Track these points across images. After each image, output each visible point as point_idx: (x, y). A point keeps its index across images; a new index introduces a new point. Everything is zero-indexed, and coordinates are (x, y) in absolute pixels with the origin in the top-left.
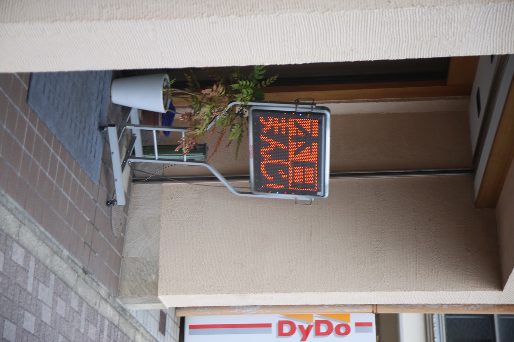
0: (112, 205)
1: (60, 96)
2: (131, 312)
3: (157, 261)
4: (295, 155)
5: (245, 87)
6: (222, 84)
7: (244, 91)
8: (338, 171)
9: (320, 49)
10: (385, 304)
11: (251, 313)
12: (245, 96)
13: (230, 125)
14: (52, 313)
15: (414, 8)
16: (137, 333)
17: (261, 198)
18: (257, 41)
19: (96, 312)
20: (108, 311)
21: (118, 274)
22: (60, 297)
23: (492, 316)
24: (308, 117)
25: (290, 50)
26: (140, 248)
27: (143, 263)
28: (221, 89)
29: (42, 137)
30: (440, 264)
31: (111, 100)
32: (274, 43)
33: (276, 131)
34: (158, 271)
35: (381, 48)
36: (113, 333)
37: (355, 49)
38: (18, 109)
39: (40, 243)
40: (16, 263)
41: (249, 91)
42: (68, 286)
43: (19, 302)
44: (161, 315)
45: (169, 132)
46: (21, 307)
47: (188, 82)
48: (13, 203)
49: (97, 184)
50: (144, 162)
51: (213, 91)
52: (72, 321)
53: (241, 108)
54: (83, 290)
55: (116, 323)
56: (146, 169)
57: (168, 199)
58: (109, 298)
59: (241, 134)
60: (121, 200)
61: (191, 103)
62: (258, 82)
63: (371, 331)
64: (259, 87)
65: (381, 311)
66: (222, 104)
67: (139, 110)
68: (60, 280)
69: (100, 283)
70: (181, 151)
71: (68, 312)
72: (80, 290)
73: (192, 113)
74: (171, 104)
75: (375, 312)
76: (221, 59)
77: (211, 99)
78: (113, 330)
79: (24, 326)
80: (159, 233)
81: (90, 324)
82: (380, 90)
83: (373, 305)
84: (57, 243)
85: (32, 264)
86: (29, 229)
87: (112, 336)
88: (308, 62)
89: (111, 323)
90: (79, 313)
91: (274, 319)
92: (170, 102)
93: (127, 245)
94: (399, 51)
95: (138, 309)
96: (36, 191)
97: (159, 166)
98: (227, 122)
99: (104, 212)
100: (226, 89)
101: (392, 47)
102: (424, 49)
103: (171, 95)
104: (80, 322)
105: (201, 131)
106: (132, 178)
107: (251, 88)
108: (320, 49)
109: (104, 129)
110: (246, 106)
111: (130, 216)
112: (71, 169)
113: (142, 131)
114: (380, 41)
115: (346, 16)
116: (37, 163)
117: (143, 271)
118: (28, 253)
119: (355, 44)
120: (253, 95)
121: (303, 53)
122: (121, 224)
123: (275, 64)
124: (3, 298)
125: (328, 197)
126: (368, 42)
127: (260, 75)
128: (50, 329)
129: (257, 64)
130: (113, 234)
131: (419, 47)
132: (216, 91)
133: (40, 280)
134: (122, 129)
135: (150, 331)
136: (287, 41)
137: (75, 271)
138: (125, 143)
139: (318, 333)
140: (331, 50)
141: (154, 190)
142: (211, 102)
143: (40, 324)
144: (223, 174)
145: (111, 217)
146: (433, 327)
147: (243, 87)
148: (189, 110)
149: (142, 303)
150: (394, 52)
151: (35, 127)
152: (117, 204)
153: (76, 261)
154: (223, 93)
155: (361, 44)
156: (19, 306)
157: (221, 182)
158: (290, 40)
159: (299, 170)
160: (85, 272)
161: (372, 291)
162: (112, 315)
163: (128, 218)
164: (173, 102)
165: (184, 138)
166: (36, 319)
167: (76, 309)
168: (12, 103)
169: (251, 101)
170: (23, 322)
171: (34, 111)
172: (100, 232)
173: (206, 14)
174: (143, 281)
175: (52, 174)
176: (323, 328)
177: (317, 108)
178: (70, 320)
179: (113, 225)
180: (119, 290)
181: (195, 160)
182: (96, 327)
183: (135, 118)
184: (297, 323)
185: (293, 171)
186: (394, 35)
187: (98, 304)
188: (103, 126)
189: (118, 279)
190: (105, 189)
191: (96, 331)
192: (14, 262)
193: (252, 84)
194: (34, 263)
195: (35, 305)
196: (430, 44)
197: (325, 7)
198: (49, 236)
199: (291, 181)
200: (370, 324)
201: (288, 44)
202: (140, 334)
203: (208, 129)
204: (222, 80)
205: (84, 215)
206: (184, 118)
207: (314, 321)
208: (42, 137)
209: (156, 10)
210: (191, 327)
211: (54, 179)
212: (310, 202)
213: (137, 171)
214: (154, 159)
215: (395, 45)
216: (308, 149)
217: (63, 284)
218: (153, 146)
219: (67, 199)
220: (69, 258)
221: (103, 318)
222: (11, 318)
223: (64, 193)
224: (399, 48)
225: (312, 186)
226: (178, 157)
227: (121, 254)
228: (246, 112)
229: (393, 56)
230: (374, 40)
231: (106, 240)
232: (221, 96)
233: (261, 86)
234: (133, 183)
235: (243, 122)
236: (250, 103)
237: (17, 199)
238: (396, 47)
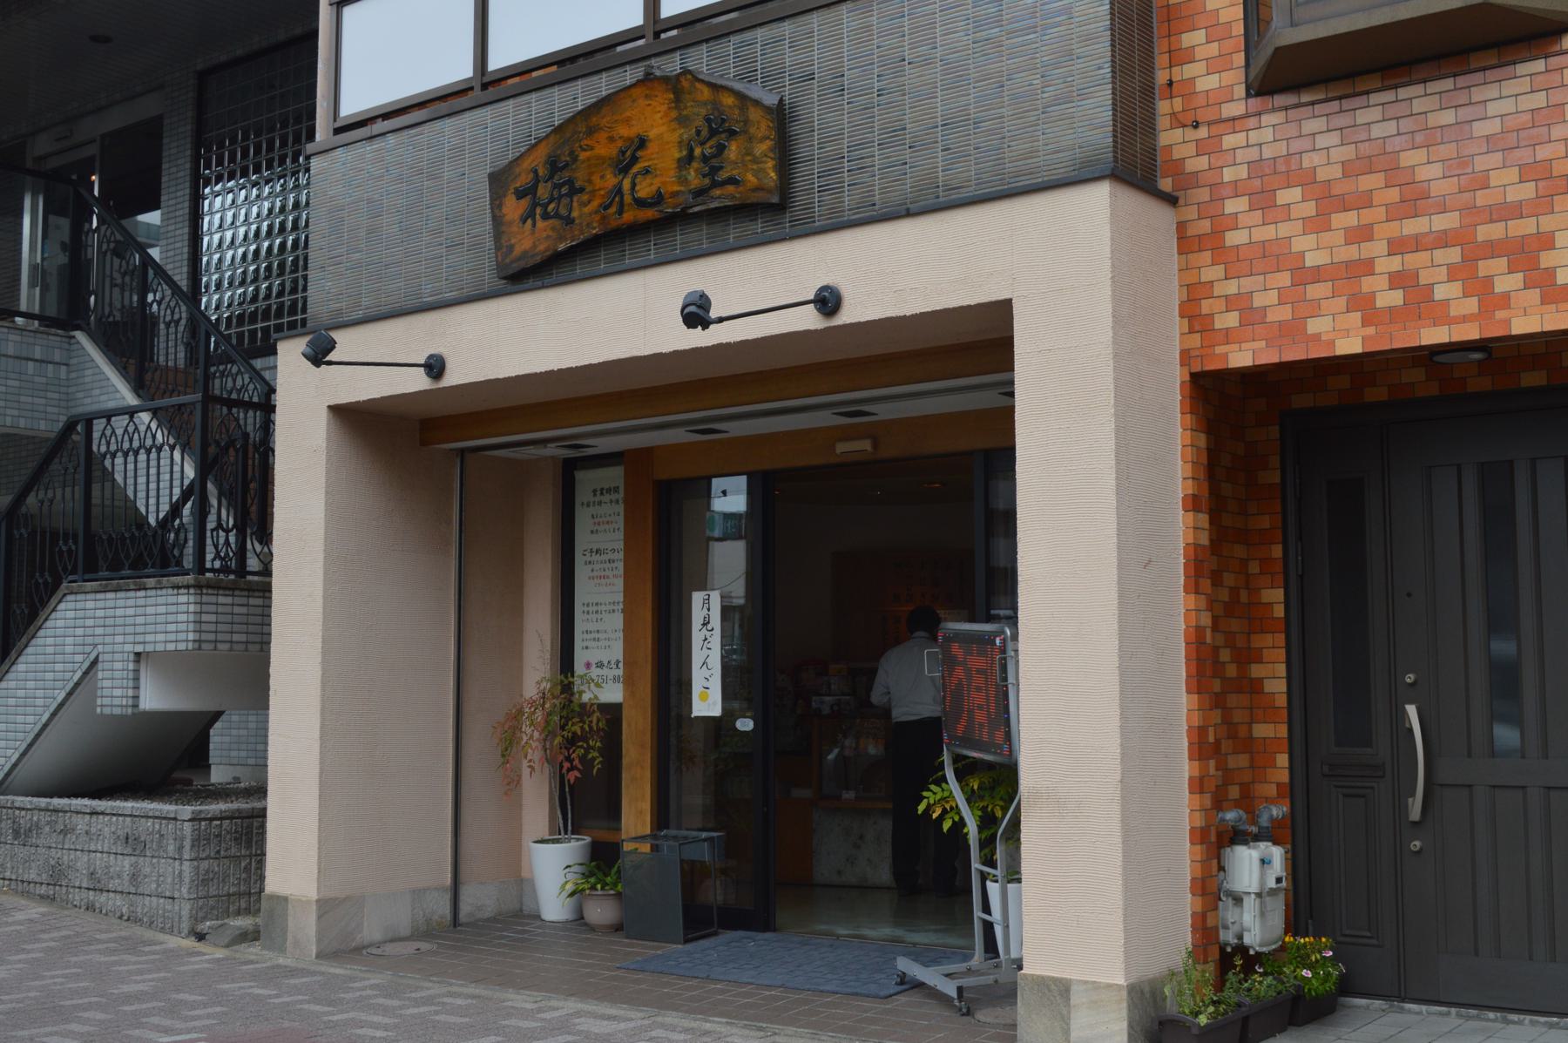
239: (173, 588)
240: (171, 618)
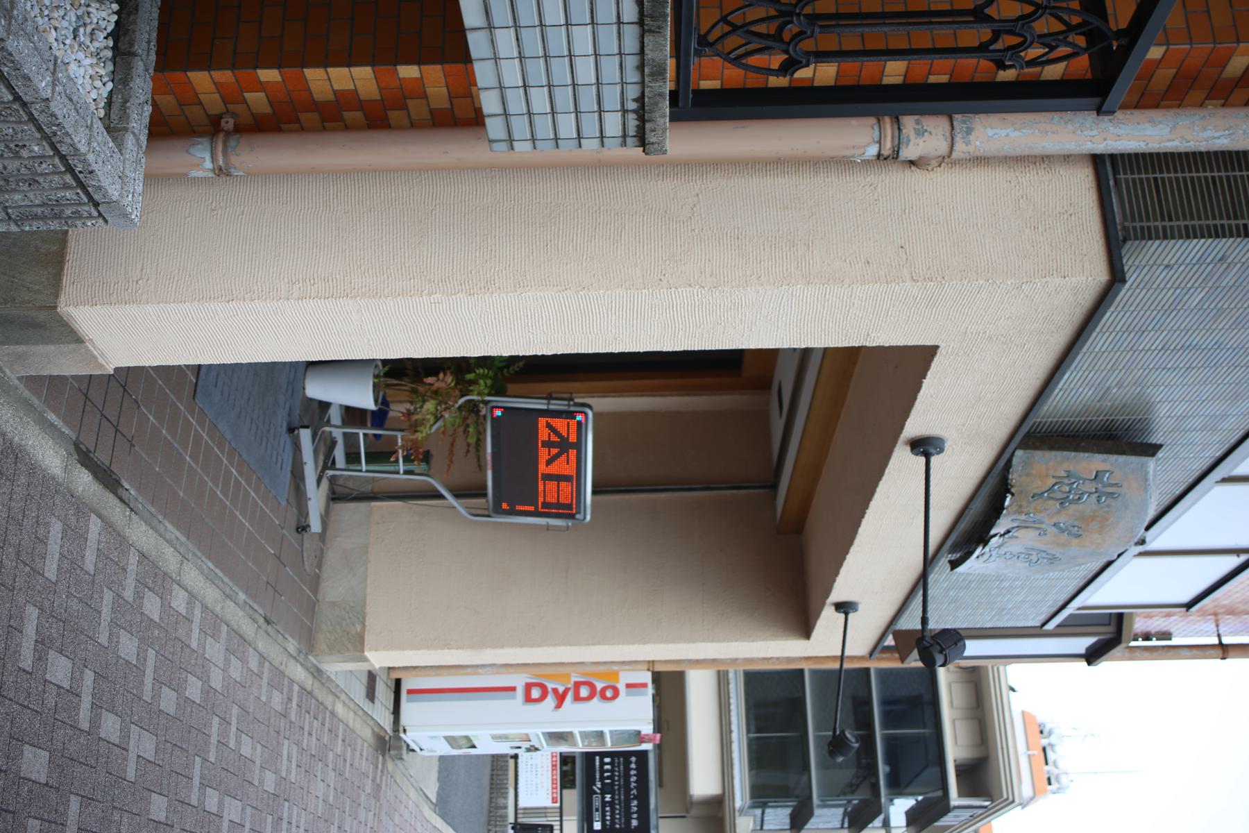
0: (303, 532)
1: (237, 390)
2: (328, 674)
3: (364, 606)
4: (547, 466)
6: (451, 373)
7: (481, 382)
12: (482, 388)
15: (692, 289)
16: (337, 700)
17: (501, 523)
19: (282, 674)
20: (298, 672)
21: (312, 623)
23: (802, 671)
27: (345, 609)
28: (449, 378)
29: (212, 444)
31: (304, 393)
34: (364, 618)
36: (304, 701)
38: (182, 408)
40: (177, 611)
42: (245, 641)
43: (181, 662)
44: (369, 677)
48: (172, 532)
52: (250, 687)
55: (309, 688)
56: (350, 484)
57: (378, 523)
58: (299, 655)
60: (315, 525)
63: (646, 694)
65: (658, 668)
67: (341, 406)
68: (235, 633)
69: (287, 636)
72: (261, 646)
74: (384, 398)
75: (651, 669)
78: (304, 697)
80: (367, 569)
82: (657, 382)
83: (649, 662)
84: (231, 584)
85: (197, 612)
87: (304, 705)
89: (302, 688)
90: (260, 676)
91: (519, 681)
93: (325, 585)
95: (338, 669)
97: (367, 480)
100: (457, 379)
104: (261, 688)
105: (424, 435)
106: (330, 495)
107: (490, 378)
112: (250, 485)
113: (345, 434)
115: (606, 297)
116: (206, 478)
117: (344, 619)
118: (192, 597)
120: (492, 387)
123: (517, 354)
124: (160, 657)
130: (305, 570)
132: (443, 381)
137: (255, 621)
138: (322, 449)
139: (577, 698)
143: (208, 691)
144: (451, 490)
146: (728, 684)
151: (204, 431)
153: (256, 607)
154: (453, 384)
156: (181, 668)
159: (552, 485)
160: (268, 622)
163: (324, 548)
168: (175, 400)
169: (490, 394)
171: (202, 410)
172: (287, 568)
173: (426, 292)
176: (584, 692)
177: (576, 405)
179: (305, 559)
182: (282, 693)
183: (335, 416)
184: (550, 686)
185: (544, 487)
187: (284, 663)
189: (312, 630)
190: (295, 510)
191: (282, 699)
197: (580, 285)
198: (220, 574)
200: (645, 685)
205: (266, 546)
207: (572, 683)
208: (212, 444)
209: (362, 287)
210: (410, 692)
211: (227, 500)
214: (361, 471)
216: (564, 457)
218: (359, 454)
219: (245, 525)
220: (246, 602)
221: (292, 681)
223: (241, 517)
225: (569, 507)
231: (296, 578)
237: (178, 527)
239: (641, 99)
240: (564, 98)
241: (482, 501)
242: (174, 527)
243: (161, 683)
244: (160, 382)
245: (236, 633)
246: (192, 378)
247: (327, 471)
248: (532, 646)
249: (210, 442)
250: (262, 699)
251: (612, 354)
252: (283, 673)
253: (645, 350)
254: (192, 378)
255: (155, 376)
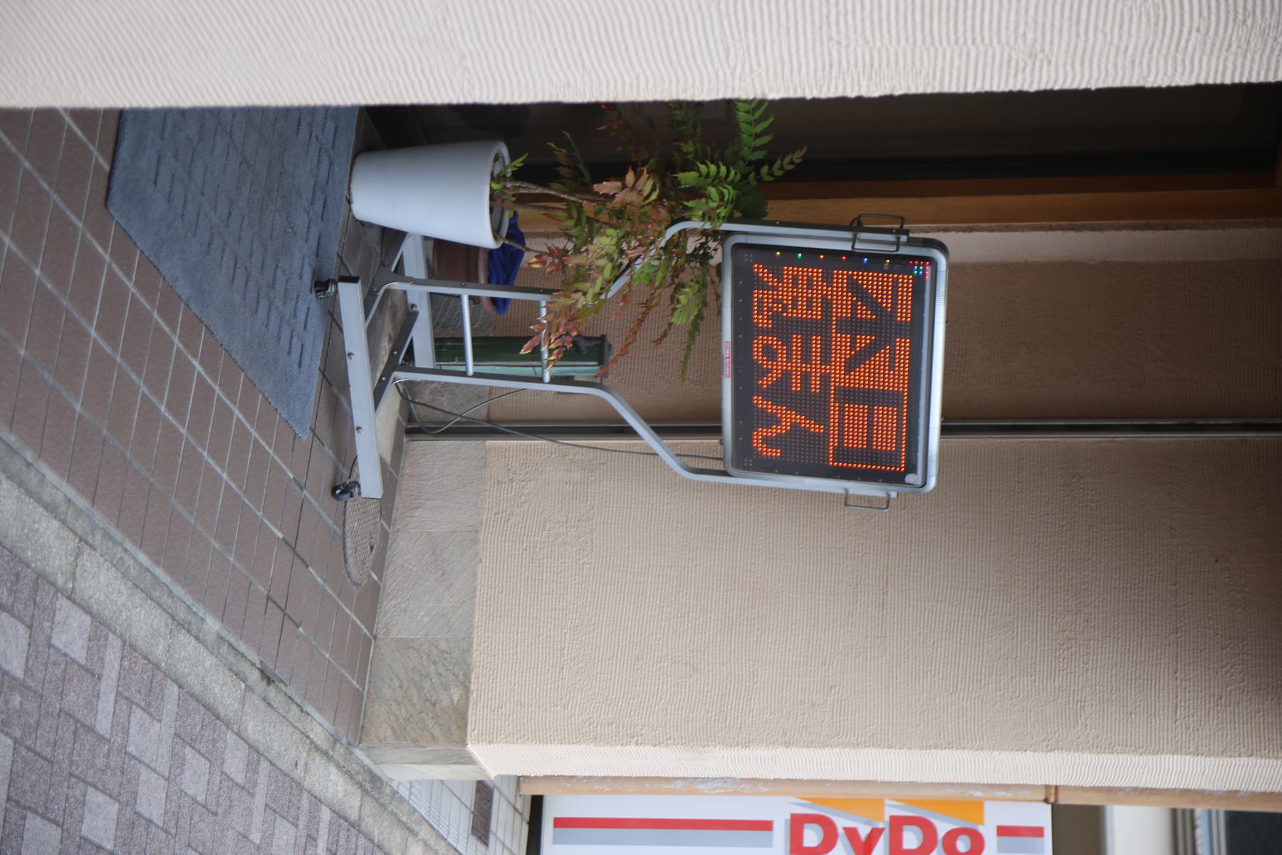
0: (346, 496)
2: (395, 784)
3: (468, 651)
4: (847, 372)
5: (714, 180)
7: (712, 191)
8: (965, 419)
9: (936, 51)
10: (1087, 784)
11: (717, 791)
12: (713, 205)
13: (670, 286)
14: (167, 794)
17: (750, 488)
18: (746, 24)
22: (193, 747)
24: (886, 267)
25: (843, 52)
26: (422, 613)
27: (428, 656)
28: (647, 184)
30: (1243, 680)
31: (350, 210)
32: (796, 30)
33: (796, 386)
34: (467, 677)
35: (1122, 48)
36: (342, 841)
37: (1043, 51)
39: (138, 598)
40: (65, 655)
41: (725, 191)
42: (218, 717)
43: (71, 762)
44: (478, 791)
45: (505, 301)
46: (76, 777)
47: (560, 165)
48: (58, 487)
49: (304, 439)
50: (439, 382)
51: (624, 187)
52: (226, 813)
53: (701, 241)
54: (259, 728)
55: (353, 816)
56: (444, 402)
58: (333, 749)
59: (700, 311)
60: (370, 483)
61: (563, 224)
62: (750, 168)
64: (754, 183)
65: (1065, 800)
66: (650, 226)
67: (426, 238)
68: (194, 699)
69: (309, 709)
70: (536, 354)
71: (216, 789)
72: (252, 728)
73: (568, 251)
74: (513, 226)
75: (1052, 799)
76: (638, 77)
77: (620, 214)
78: (343, 834)
79: (85, 830)
80: (475, 575)
81: (279, 819)
82: (1086, 198)
83: (1047, 787)
84: (189, 600)
85: (112, 657)
86: (106, 560)
88: (898, 92)
89: (339, 815)
90: (248, 790)
91: (780, 811)
92: (511, 219)
93: (387, 606)
94: (1175, 58)
95: (413, 778)
96: (128, 455)
97: (478, 393)
98: (664, 278)
99: (323, 514)
100: (663, 185)
101: (1157, 44)
102: (1255, 53)
103: (514, 199)
106: (404, 424)
107: (731, 183)
108: (936, 51)
109: (327, 289)
110: (715, 234)
111: (397, 527)
113: (432, 295)
114: (1121, 27)
117: (427, 676)
118: (101, 625)
119: (1043, 34)
120: (736, 203)
121: (884, 63)
122: (372, 548)
123: (799, 95)
124: (24, 752)
125: (935, 488)
126: (1082, 31)
127: (755, 149)
128: (163, 835)
129: (744, 97)
131: (1239, 47)
133: (136, 701)
134: (378, 291)
135: (448, 834)
136: (838, 24)
138: (387, 329)
140: (968, 54)
141: (464, 459)
142: (620, 221)
143: (132, 823)
144: (647, 419)
145: (344, 528)
146: (1194, 828)
147: (709, 180)
148: (560, 243)
149: (424, 763)
150: (1162, 62)
151: (130, 278)
152: (360, 494)
153: (242, 647)
154: (654, 196)
155: (1060, 36)
156: (71, 775)
157: (642, 439)
158: (846, 22)
159: (856, 412)
160: (268, 678)
161: (1050, 751)
162: (341, 795)
164: (519, 220)
165: (544, 318)
166: (120, 810)
167: (240, 779)
168: (62, 205)
169: (730, 219)
170: (82, 820)
174: (428, 704)
175: (177, 407)
178: (220, 810)
179: (349, 552)
180: (363, 727)
181: (576, 379)
182: (297, 826)
183: (414, 259)
184: (841, 823)
186: (1164, 8)
187: (301, 763)
188: (325, 279)
192: (58, 650)
193: (733, 172)
194: (119, 655)
195: (118, 772)
196: (1275, 39)
199: (833, 443)
200: (1037, 832)
201: (839, 32)
202: (421, 843)
203: (610, 295)
204: (652, 160)
206: (544, 263)
207: (887, 819)
210: (560, 823)
211: (183, 423)
212: (885, 502)
213: (419, 407)
214: (464, 374)
215: (1166, 41)
216: (882, 356)
217: (202, 712)
219: (220, 478)
220: (221, 638)
221: (317, 800)
222: (47, 808)
223: (211, 462)
224: (1177, 51)
225: (891, 457)
226: (531, 369)
227: (371, 630)
228: (715, 250)
229: (1157, 75)
230: (1100, 24)
232: (649, 203)
233: (760, 180)
234: (408, 439)
235: (708, 279)
236: (726, 227)
237: (70, 478)
238: (1169, 47)
241: (713, 441)
242: (62, 475)
243: (25, 808)
244: (27, 164)
245: (198, 701)
246: (101, 160)
247: (396, 374)
248: (810, 745)
249: (143, 300)
250: (252, 837)
251: (1022, 95)
252: (299, 784)
253: (1101, 85)
254: (101, 160)
255: (13, 149)
